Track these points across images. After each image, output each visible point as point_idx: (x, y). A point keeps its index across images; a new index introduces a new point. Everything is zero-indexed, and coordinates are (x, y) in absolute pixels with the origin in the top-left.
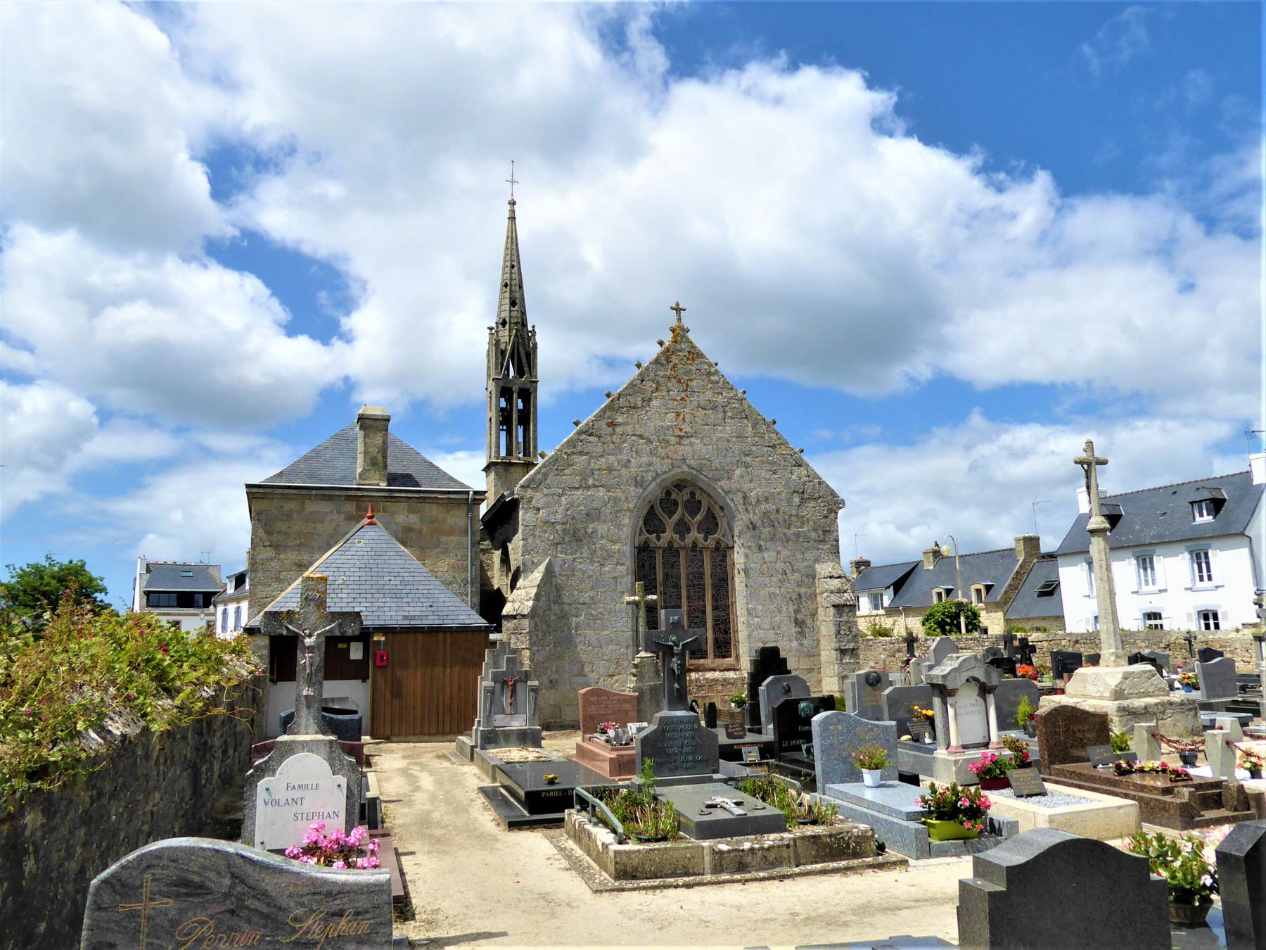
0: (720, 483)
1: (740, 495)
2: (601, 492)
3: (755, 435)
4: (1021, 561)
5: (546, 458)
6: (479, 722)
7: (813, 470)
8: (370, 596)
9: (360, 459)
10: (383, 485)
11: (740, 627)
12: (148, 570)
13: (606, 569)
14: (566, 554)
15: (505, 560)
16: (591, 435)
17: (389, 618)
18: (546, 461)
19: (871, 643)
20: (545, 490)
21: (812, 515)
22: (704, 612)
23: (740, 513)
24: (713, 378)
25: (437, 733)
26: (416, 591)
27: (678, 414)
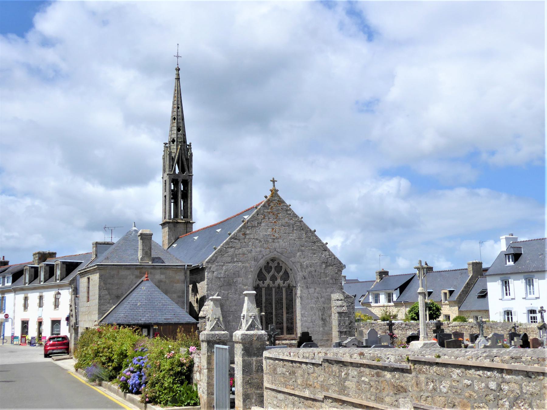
1: (299, 264)
4: (470, 276)
16: (236, 239)
17: (159, 319)
19: (374, 325)
20: (216, 263)
22: (282, 315)
23: (299, 272)
24: (288, 212)
27: (273, 229)
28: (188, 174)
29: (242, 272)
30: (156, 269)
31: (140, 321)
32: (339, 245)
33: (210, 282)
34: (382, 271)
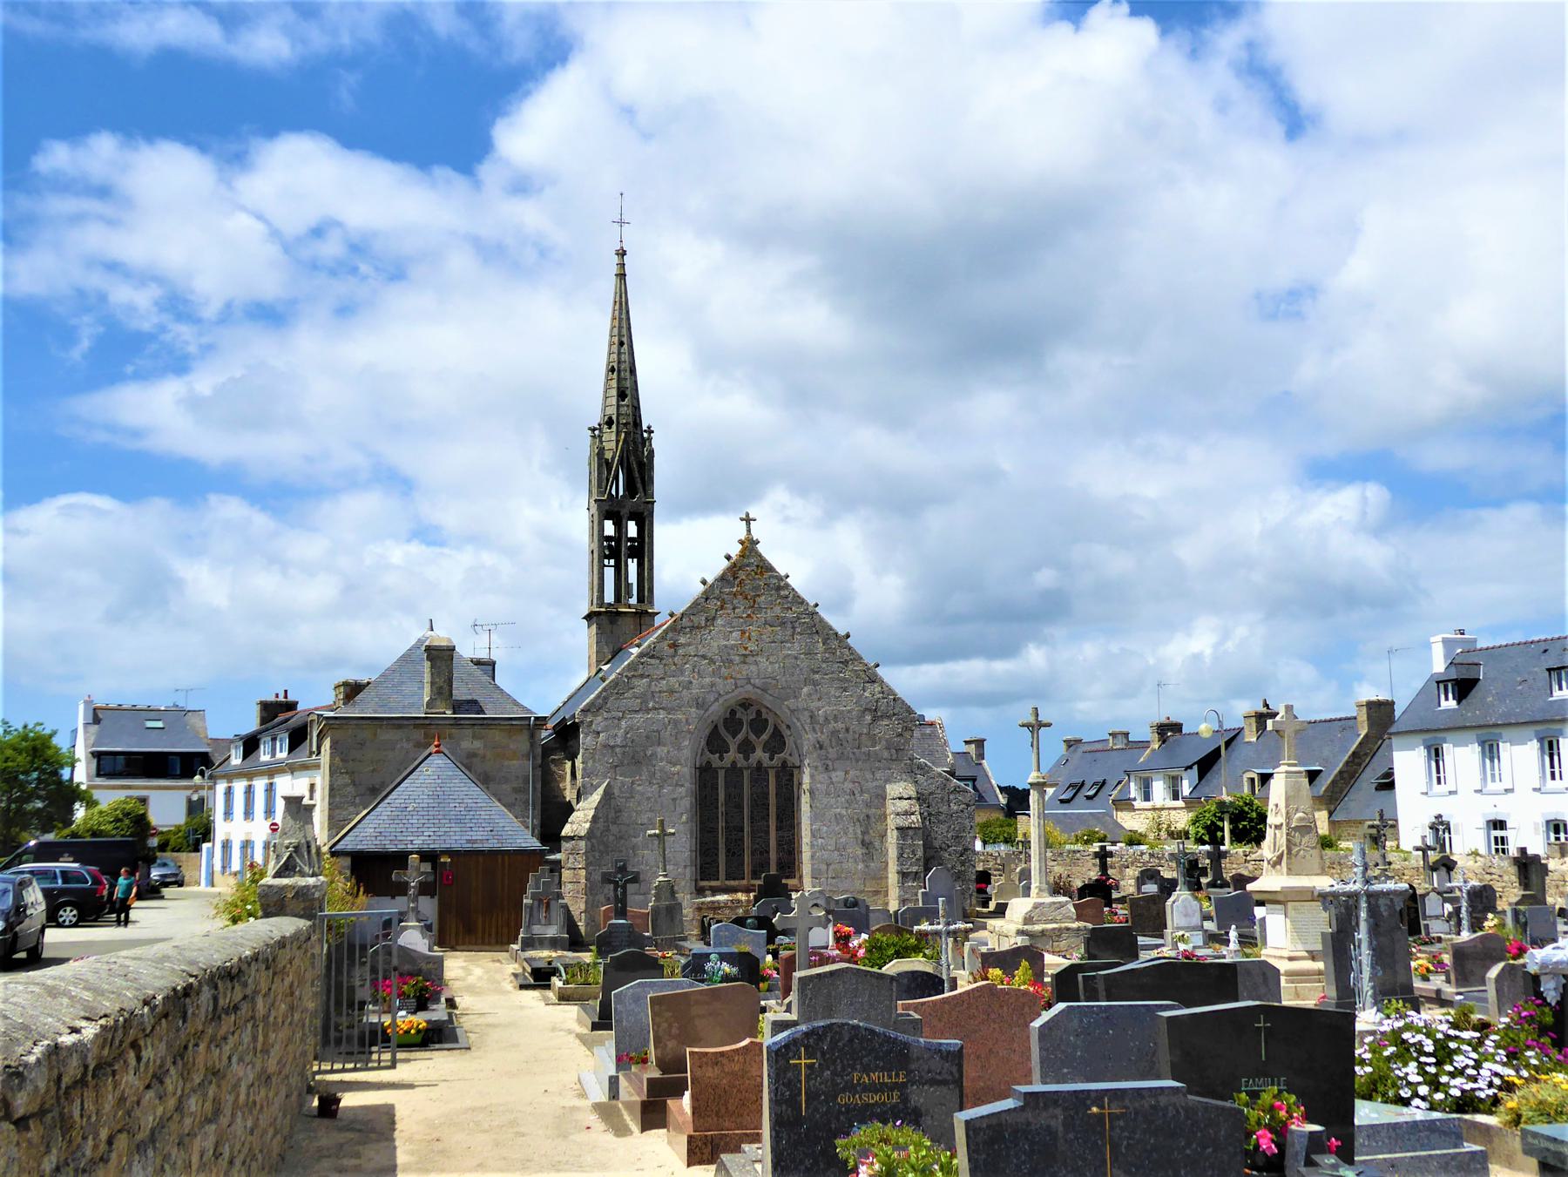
2: (662, 715)
9: (427, 690)
10: (449, 714)
12: (96, 720)
16: (653, 657)
19: (1078, 855)
22: (767, 833)
24: (782, 593)
27: (743, 632)
28: (643, 500)
29: (666, 734)
31: (409, 846)
32: (1208, 652)
33: (591, 755)
34: (1167, 721)
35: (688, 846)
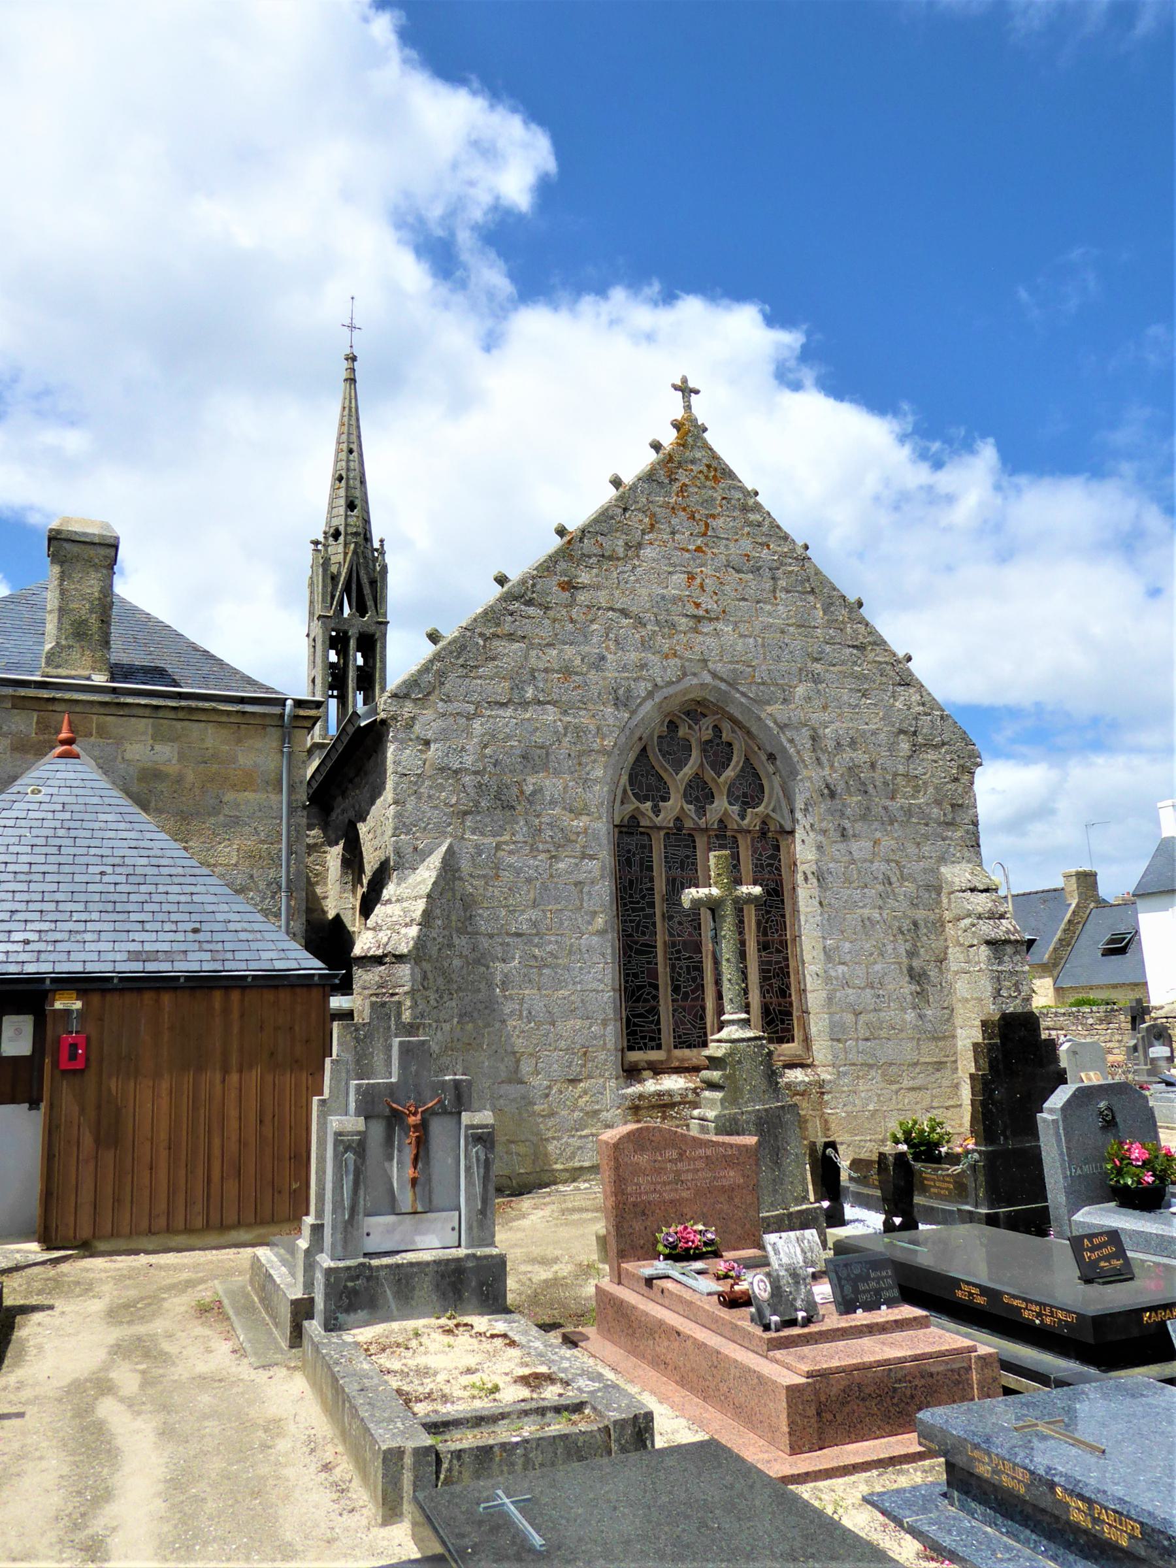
0: (769, 709)
2: (551, 714)
3: (830, 623)
5: (441, 644)
6: (317, 1229)
7: (929, 694)
8: (52, 906)
9: (51, 627)
11: (810, 983)
13: (561, 865)
14: (482, 834)
15: (353, 861)
16: (529, 603)
18: (444, 649)
20: (441, 704)
21: (933, 776)
23: (806, 767)
24: (752, 517)
25: (207, 1227)
26: (162, 898)
27: (691, 577)
30: (126, 711)
35: (608, 979)
